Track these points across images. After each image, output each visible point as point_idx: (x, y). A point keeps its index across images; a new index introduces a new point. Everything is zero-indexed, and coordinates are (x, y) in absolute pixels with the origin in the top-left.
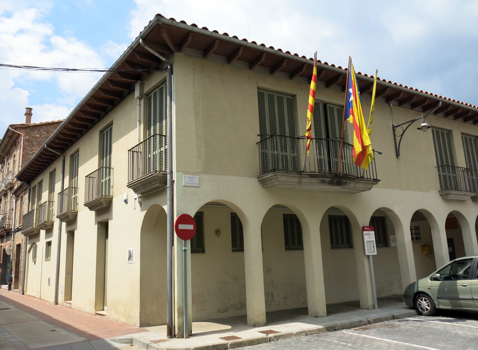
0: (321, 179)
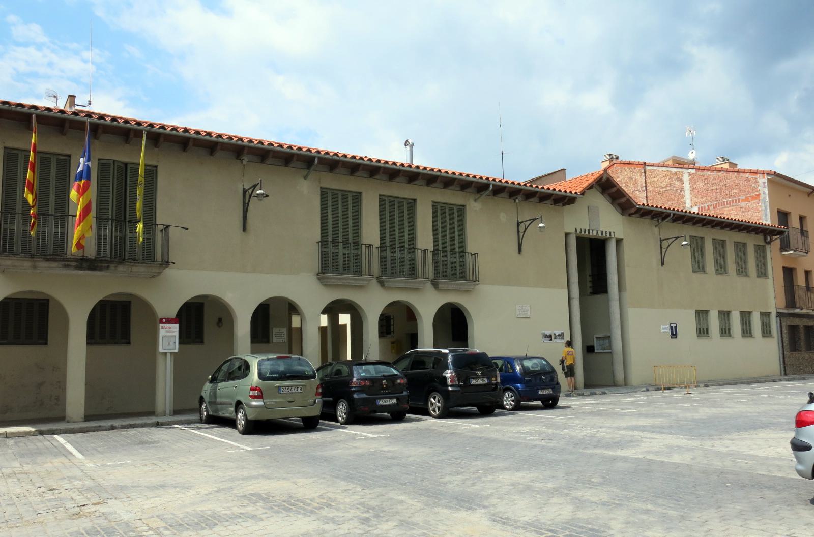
0: (63, 263)
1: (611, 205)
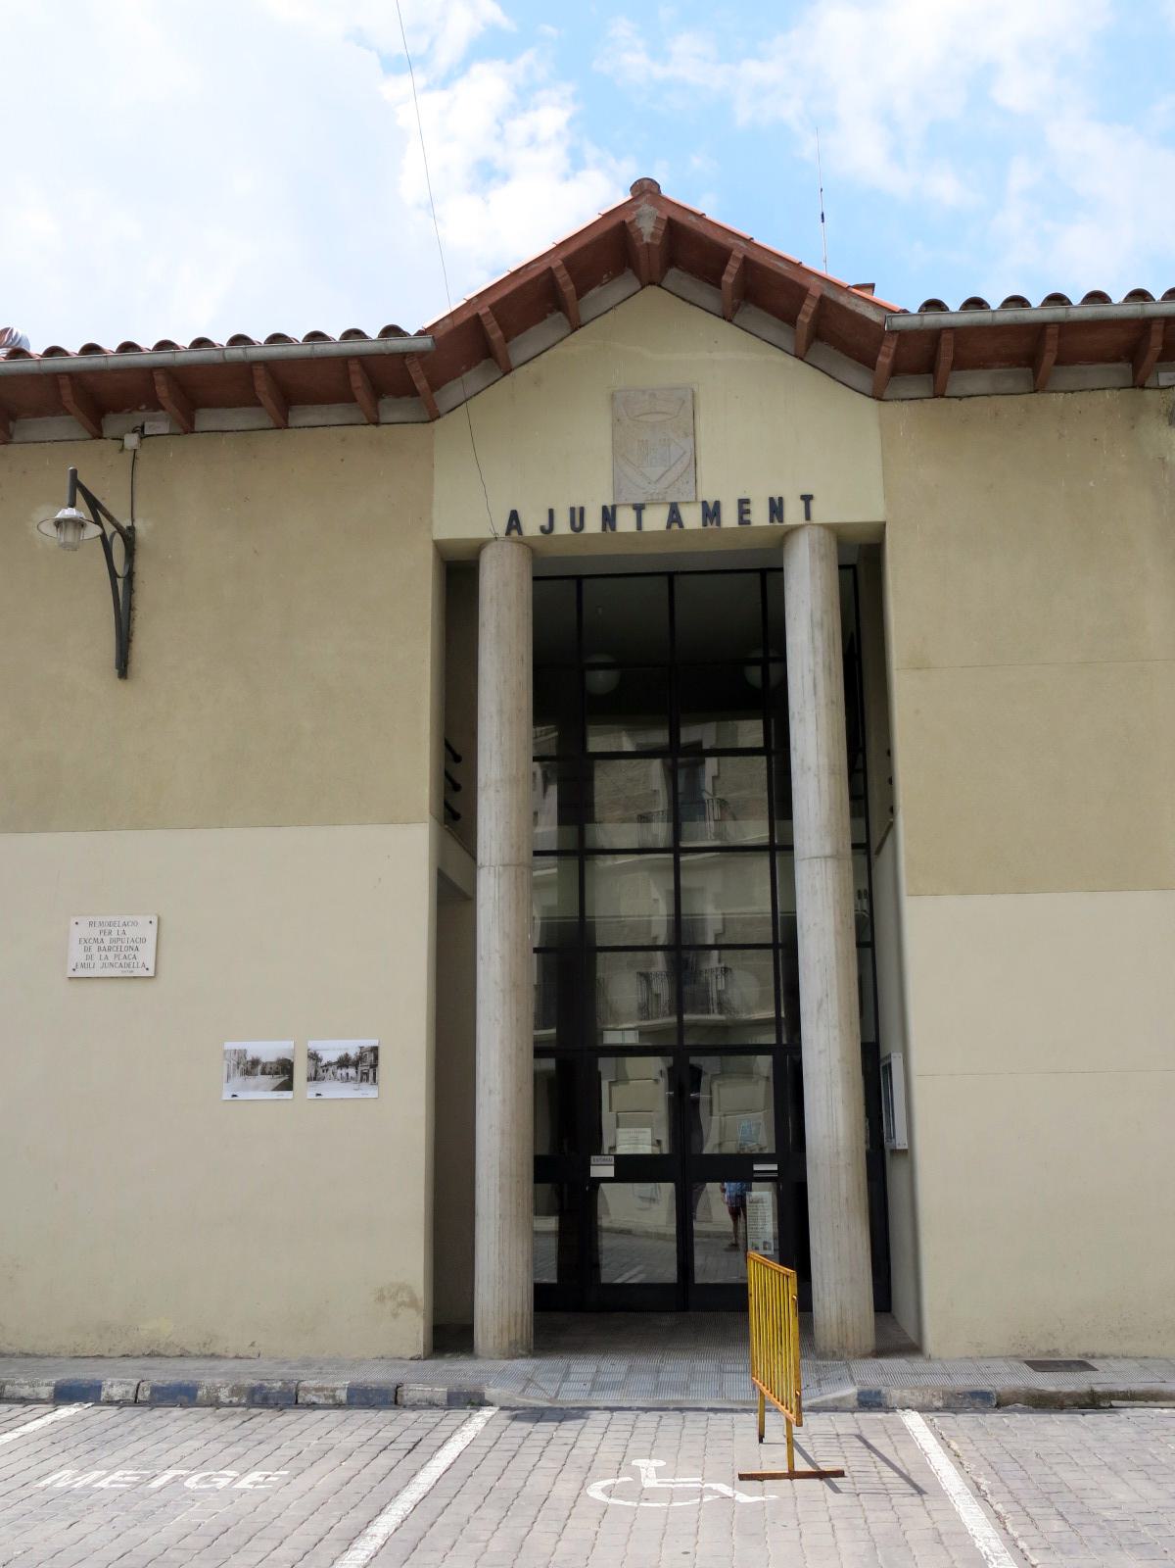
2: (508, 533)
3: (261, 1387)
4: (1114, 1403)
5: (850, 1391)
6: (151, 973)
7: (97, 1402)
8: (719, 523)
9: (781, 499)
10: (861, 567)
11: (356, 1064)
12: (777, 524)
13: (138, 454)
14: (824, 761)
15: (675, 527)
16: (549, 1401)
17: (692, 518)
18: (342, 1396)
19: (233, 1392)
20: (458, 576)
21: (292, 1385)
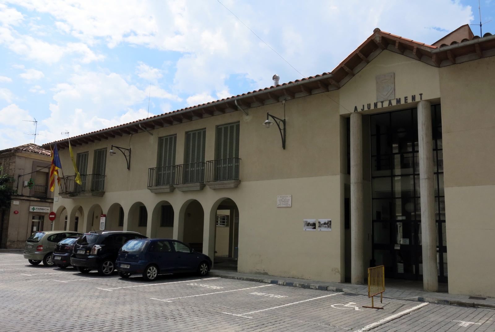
1: (418, 62)
2: (355, 111)
3: (304, 284)
4: (479, 307)
5: (417, 297)
6: (290, 206)
7: (277, 284)
8: (400, 103)
9: (415, 96)
10: (435, 108)
11: (327, 224)
12: (414, 101)
13: (286, 104)
14: (425, 157)
15: (390, 105)
16: (356, 293)
17: (394, 103)
18: (317, 287)
19: (299, 285)
20: (346, 120)
21: (309, 285)
